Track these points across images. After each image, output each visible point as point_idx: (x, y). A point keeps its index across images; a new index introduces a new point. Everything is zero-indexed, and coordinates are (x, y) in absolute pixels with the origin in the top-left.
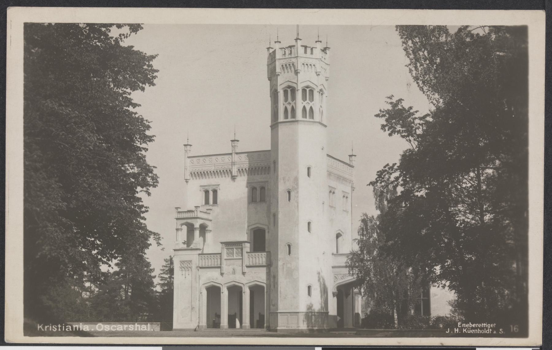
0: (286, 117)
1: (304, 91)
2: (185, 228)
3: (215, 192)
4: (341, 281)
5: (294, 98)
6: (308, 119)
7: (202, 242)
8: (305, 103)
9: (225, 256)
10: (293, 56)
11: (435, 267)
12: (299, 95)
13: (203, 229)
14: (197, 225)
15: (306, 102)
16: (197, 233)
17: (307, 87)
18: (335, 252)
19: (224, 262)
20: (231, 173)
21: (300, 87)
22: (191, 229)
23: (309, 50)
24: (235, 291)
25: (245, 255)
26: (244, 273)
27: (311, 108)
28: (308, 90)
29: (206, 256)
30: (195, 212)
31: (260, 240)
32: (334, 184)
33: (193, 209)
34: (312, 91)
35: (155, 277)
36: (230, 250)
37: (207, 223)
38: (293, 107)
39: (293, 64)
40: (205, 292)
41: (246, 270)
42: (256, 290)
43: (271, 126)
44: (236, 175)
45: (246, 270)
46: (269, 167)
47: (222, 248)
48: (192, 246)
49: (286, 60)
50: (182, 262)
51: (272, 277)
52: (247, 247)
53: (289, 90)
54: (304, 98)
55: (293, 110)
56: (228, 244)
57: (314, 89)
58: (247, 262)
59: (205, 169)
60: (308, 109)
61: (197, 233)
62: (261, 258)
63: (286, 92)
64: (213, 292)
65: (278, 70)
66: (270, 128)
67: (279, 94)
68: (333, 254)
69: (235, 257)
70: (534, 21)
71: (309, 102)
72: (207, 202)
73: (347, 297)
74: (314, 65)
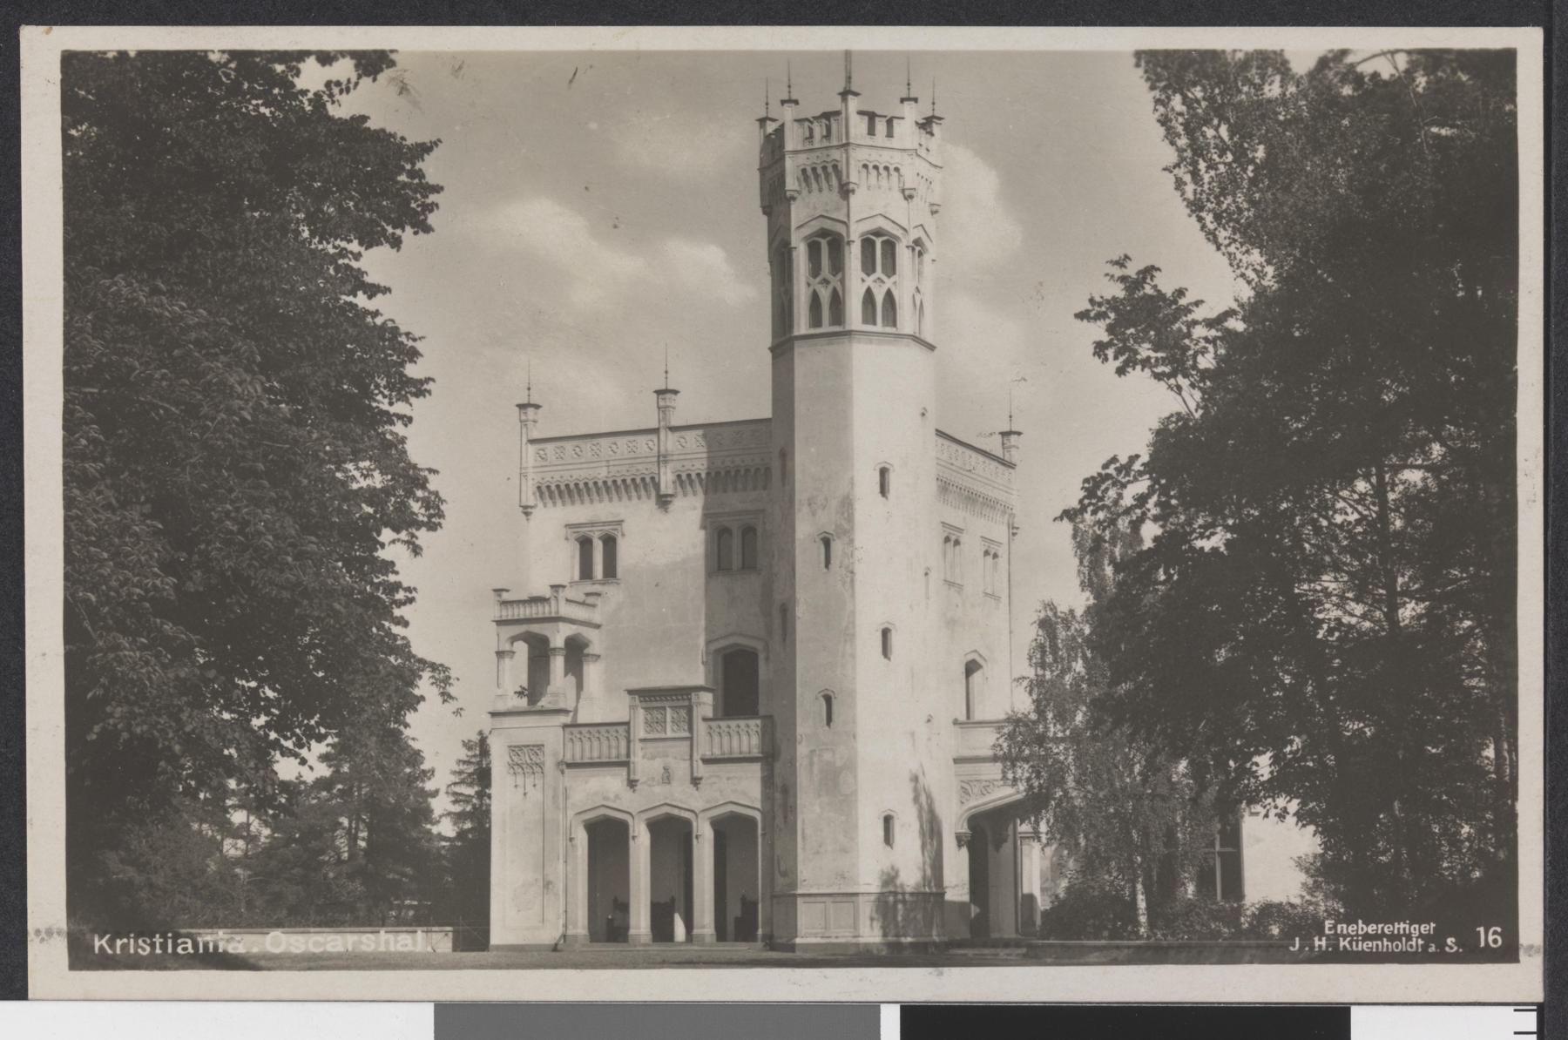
0: (816, 320)
1: (868, 244)
2: (522, 649)
6: (879, 328)
8: (870, 281)
9: (640, 731)
10: (835, 142)
14: (558, 641)
15: (874, 277)
16: (558, 664)
18: (963, 718)
19: (637, 747)
20: (657, 486)
22: (540, 652)
23: (881, 126)
24: (671, 833)
25: (701, 728)
28: (878, 242)
32: (956, 516)
34: (890, 246)
35: (435, 793)
41: (701, 770)
43: (772, 349)
46: (768, 469)
49: (813, 155)
50: (515, 749)
52: (705, 704)
53: (824, 243)
54: (869, 267)
55: (838, 302)
57: (897, 238)
58: (704, 748)
59: (580, 474)
60: (879, 298)
61: (558, 664)
62: (746, 736)
65: (791, 183)
66: (769, 355)
67: (794, 254)
68: (956, 722)
69: (669, 734)
70: (1527, 43)
71: (884, 278)
72: (586, 573)
73: (998, 847)
74: (897, 169)
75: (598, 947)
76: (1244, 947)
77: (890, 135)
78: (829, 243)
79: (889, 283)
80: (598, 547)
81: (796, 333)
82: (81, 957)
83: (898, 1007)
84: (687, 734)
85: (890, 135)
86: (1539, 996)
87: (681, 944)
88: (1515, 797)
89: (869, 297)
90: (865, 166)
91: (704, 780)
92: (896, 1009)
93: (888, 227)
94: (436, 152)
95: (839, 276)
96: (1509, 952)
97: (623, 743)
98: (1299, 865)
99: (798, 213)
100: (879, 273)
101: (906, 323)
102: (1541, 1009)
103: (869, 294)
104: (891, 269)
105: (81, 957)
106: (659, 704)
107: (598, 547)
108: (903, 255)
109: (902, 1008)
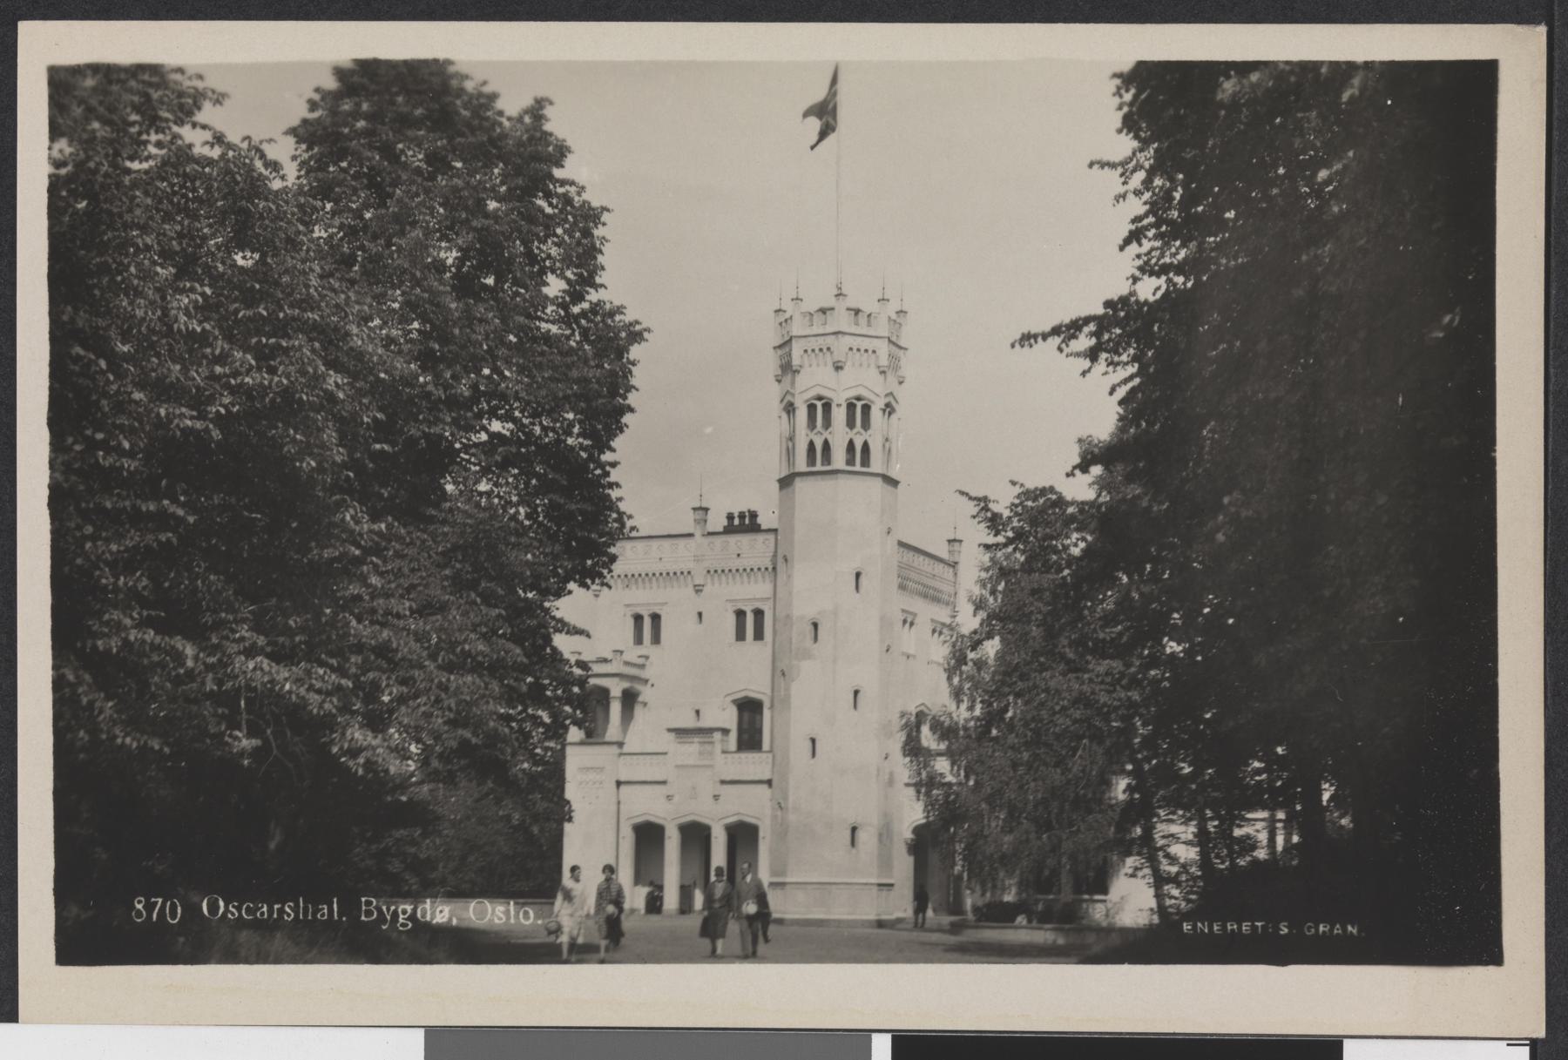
0: (850, 462)
1: (851, 407)
3: (656, 618)
5: (827, 423)
8: (851, 434)
12: (839, 415)
17: (859, 399)
21: (840, 398)
24: (696, 835)
28: (859, 404)
34: (866, 409)
37: (639, 687)
53: (819, 404)
54: (851, 423)
63: (812, 408)
70: (1518, 56)
72: (639, 640)
77: (869, 325)
79: (826, 435)
80: (647, 623)
82: (76, 946)
83: (889, 1036)
85: (869, 325)
86: (1541, 1033)
88: (1315, 66)
89: (851, 446)
92: (888, 1038)
93: (864, 393)
96: (1482, 946)
101: (876, 465)
102: (1534, 1044)
103: (811, 446)
104: (866, 424)
105: (76, 946)
107: (647, 623)
108: (876, 413)
109: (894, 1038)
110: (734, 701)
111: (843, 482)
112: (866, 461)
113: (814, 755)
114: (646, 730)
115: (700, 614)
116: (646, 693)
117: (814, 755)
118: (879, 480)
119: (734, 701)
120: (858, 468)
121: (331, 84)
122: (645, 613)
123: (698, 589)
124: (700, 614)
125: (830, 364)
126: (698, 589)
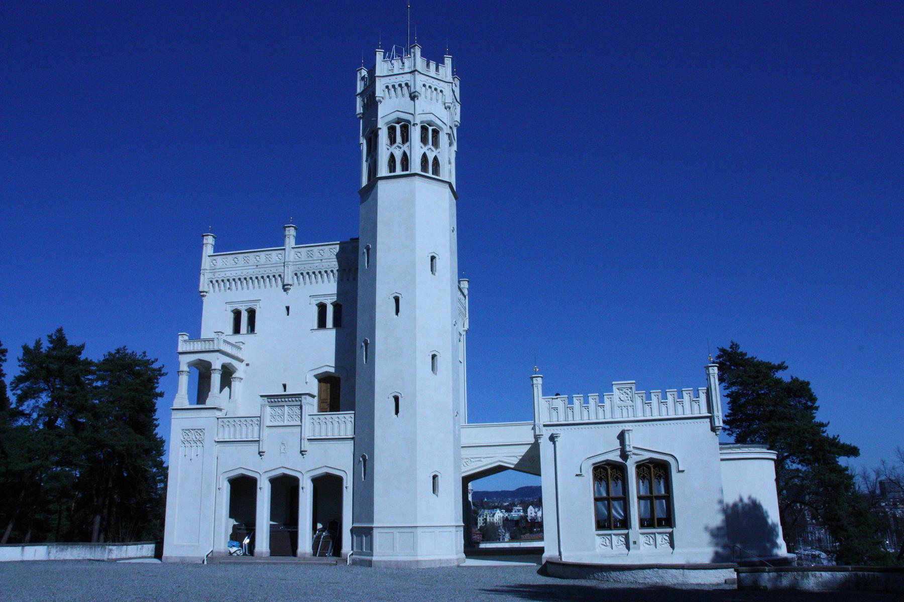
0: (392, 167)
1: (424, 129)
3: (252, 313)
4: (480, 464)
5: (406, 138)
7: (485, 588)
8: (425, 149)
9: (268, 421)
10: (407, 70)
11: (49, 399)
13: (227, 375)
19: (266, 432)
20: (282, 280)
24: (285, 488)
25: (307, 420)
26: (302, 452)
27: (436, 159)
29: (231, 420)
30: (216, 342)
31: (341, 390)
33: (213, 336)
34: (436, 133)
36: (277, 409)
37: (235, 363)
38: (405, 154)
39: (407, 84)
40: (226, 488)
41: (307, 446)
42: (328, 487)
44: (290, 283)
45: (307, 446)
47: (263, 406)
48: (209, 403)
50: (186, 431)
51: (364, 461)
52: (311, 406)
53: (398, 127)
54: (424, 140)
55: (405, 159)
56: (273, 399)
58: (308, 433)
62: (342, 423)
63: (392, 130)
64: (242, 490)
65: (379, 92)
67: (380, 132)
69: (286, 423)
71: (433, 148)
72: (237, 330)
74: (441, 91)
75: (276, 559)
76: (258, 563)
78: (401, 127)
79: (405, 148)
81: (379, 175)
84: (299, 423)
87: (304, 557)
90: (424, 85)
91: (315, 447)
94: (166, 377)
95: (408, 144)
97: (257, 428)
98: (706, 528)
99: (382, 110)
100: (430, 145)
104: (436, 143)
106: (281, 404)
110: (316, 376)
111: (418, 181)
112: (436, 170)
113: (397, 412)
114: (242, 399)
115: (288, 308)
116: (240, 371)
117: (397, 412)
118: (447, 185)
119: (316, 376)
120: (430, 174)
121: (165, 465)
122: (243, 309)
123: (286, 288)
124: (288, 308)
125: (407, 95)
126: (413, 97)
